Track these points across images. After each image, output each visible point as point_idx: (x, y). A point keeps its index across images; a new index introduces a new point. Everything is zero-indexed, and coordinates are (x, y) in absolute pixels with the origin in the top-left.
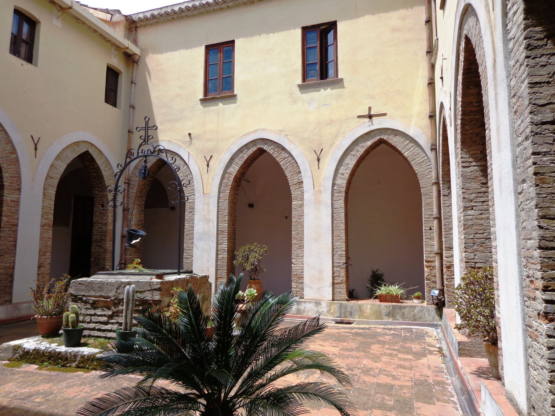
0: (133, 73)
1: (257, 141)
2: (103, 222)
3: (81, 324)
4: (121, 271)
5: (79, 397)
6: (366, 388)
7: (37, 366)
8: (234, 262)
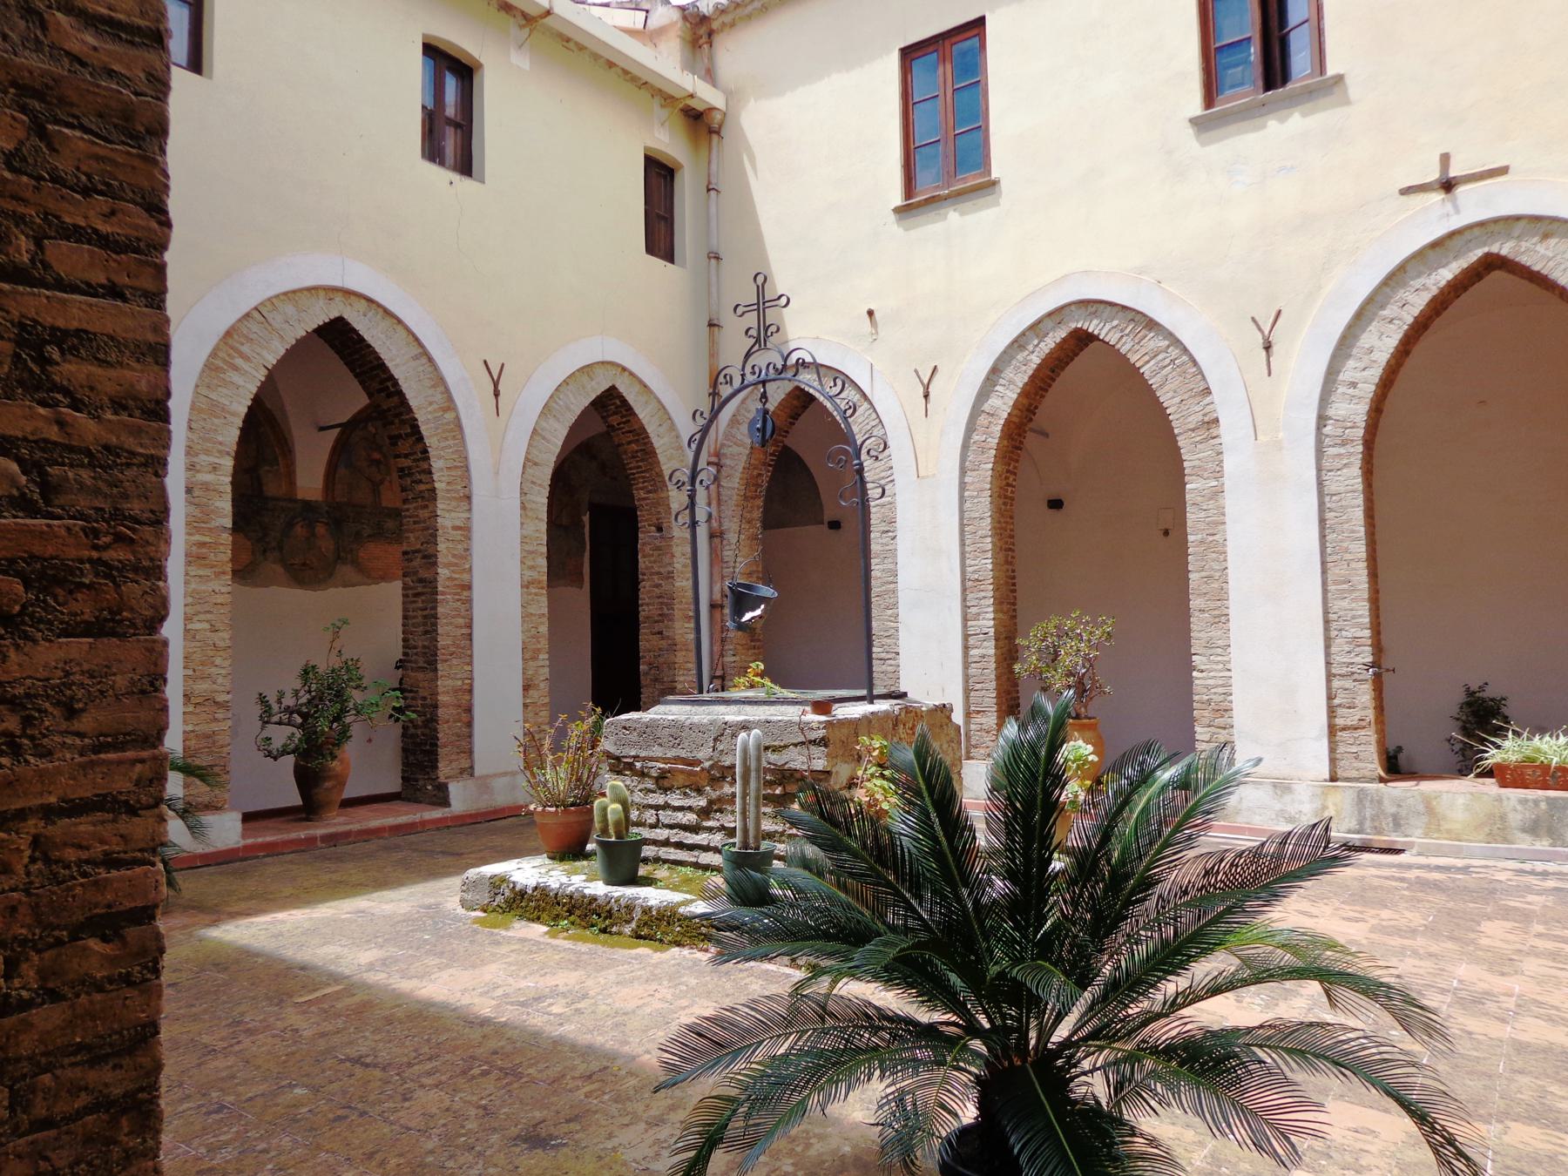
0: (709, 163)
1: (1067, 311)
2: (662, 570)
3: (635, 830)
4: (720, 694)
5: (648, 1010)
6: (1475, 1054)
7: (546, 929)
8: (1017, 667)
